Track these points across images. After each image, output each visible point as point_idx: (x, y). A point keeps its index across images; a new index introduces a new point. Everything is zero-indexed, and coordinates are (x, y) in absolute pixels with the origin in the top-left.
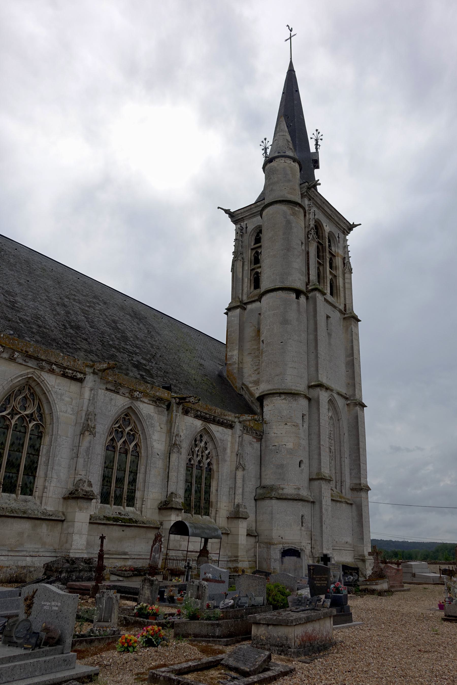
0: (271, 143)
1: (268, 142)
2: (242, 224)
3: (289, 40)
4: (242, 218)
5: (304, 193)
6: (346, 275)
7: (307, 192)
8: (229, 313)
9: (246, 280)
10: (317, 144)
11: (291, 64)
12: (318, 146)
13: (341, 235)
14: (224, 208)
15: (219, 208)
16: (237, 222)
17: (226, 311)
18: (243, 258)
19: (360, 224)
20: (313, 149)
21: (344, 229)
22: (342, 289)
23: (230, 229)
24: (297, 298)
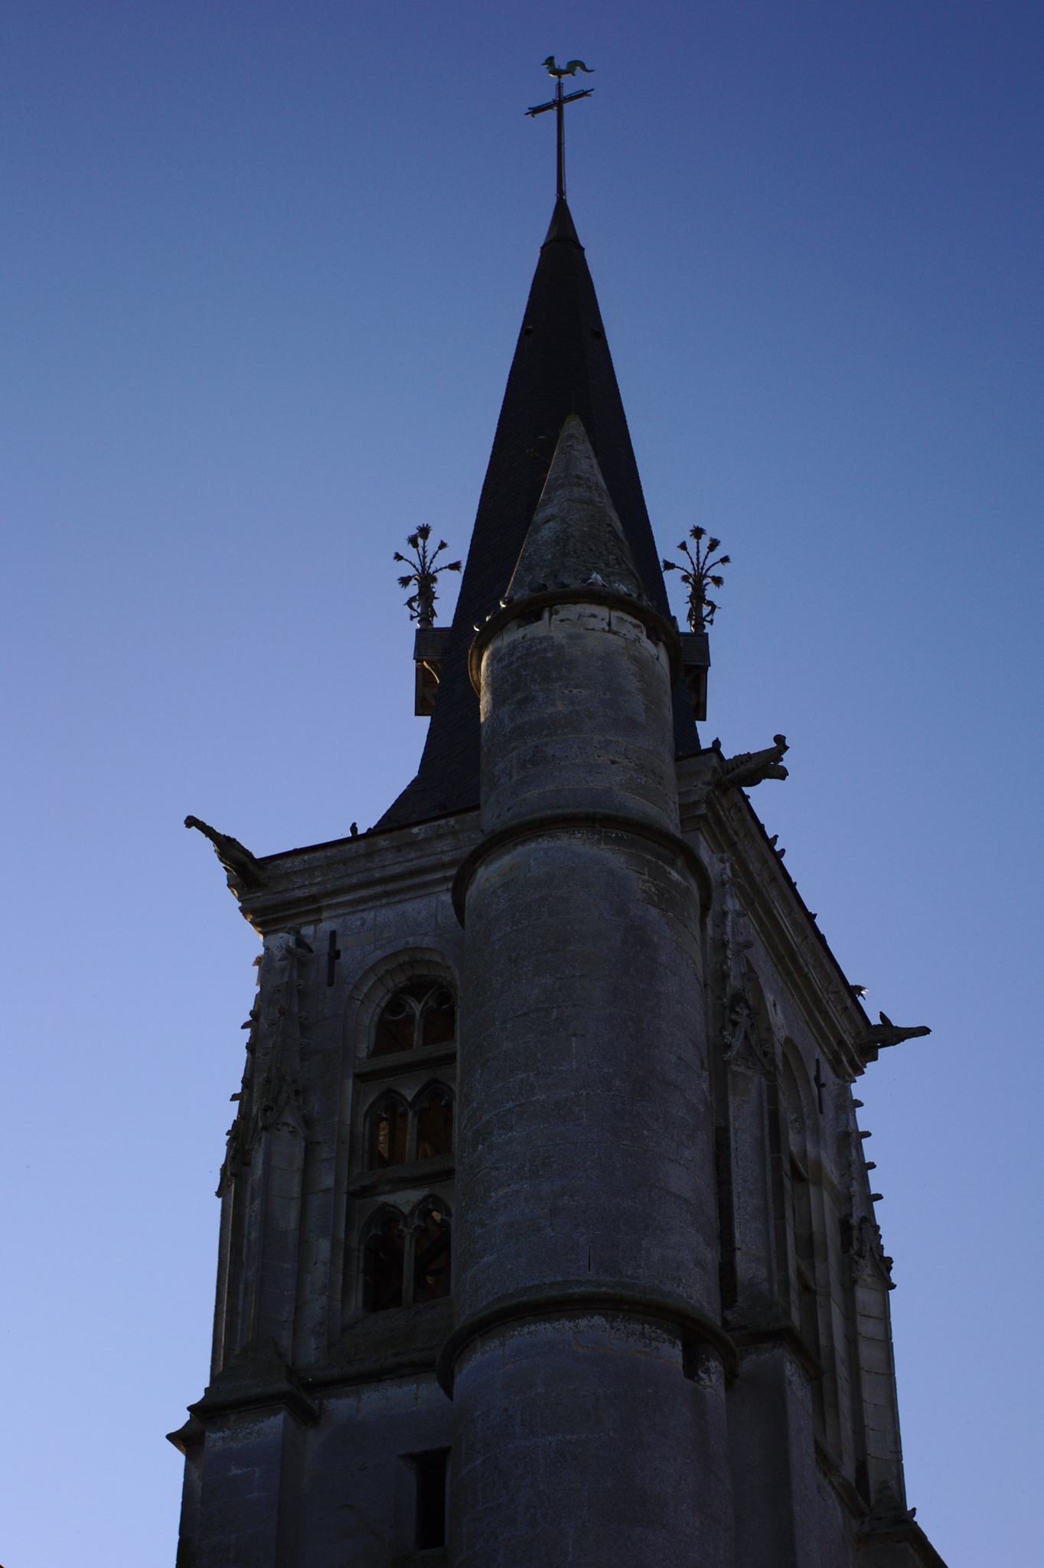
0: (460, 550)
1: (443, 545)
2: (308, 931)
3: (552, 113)
4: (313, 898)
5: (695, 804)
6: (864, 1295)
7: (709, 803)
8: (215, 1439)
9: (323, 1248)
10: (698, 597)
11: (562, 215)
12: (706, 609)
13: (828, 1074)
14: (221, 830)
15: (191, 822)
16: (276, 921)
17: (777, 848)
18: (308, 1122)
19: (924, 1031)
20: (685, 626)
21: (841, 1043)
22: (842, 1371)
23: (230, 957)
24: (692, 1367)
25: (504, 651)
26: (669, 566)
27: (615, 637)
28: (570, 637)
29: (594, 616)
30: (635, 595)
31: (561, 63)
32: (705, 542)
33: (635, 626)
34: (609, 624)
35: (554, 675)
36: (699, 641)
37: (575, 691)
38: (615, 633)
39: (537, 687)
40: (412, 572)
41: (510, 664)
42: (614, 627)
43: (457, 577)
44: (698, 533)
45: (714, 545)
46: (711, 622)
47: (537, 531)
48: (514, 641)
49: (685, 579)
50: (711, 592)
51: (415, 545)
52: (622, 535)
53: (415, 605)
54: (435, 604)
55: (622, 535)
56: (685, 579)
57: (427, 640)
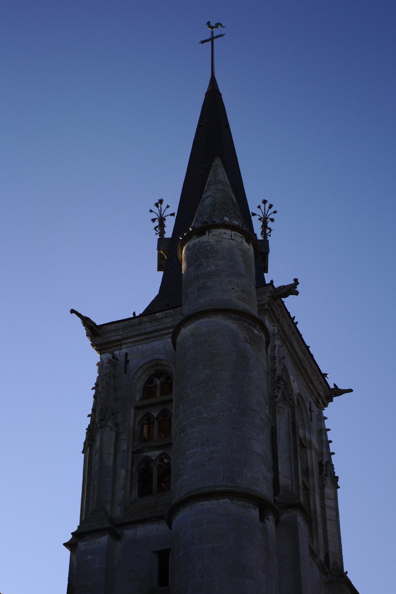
0: (174, 208)
1: (168, 207)
2: (117, 353)
3: (210, 43)
4: (119, 340)
5: (264, 305)
6: (328, 491)
7: (269, 304)
8: (82, 545)
9: (122, 473)
10: (265, 226)
11: (213, 81)
12: (268, 231)
13: (314, 407)
14: (84, 314)
15: (72, 311)
16: (105, 349)
17: (295, 321)
18: (117, 425)
19: (350, 391)
20: (260, 237)
21: (319, 395)
22: (319, 519)
23: (87, 363)
24: (262, 518)
25: (191, 246)
26: (254, 214)
27: (233, 241)
28: (216, 241)
29: (225, 233)
30: (241, 225)
31: (213, 24)
32: (267, 205)
33: (241, 237)
34: (231, 236)
35: (210, 256)
36: (265, 243)
37: (218, 262)
38: (233, 240)
39: (204, 260)
40: (156, 217)
41: (194, 251)
42: (233, 238)
43: (174, 219)
44: (265, 202)
45: (271, 206)
46: (270, 236)
47: (204, 201)
48: (195, 243)
49: (260, 219)
50: (270, 224)
51: (158, 206)
52: (236, 203)
53: (157, 229)
54: (165, 229)
55: (236, 203)
56: (260, 219)
57: (162, 242)
